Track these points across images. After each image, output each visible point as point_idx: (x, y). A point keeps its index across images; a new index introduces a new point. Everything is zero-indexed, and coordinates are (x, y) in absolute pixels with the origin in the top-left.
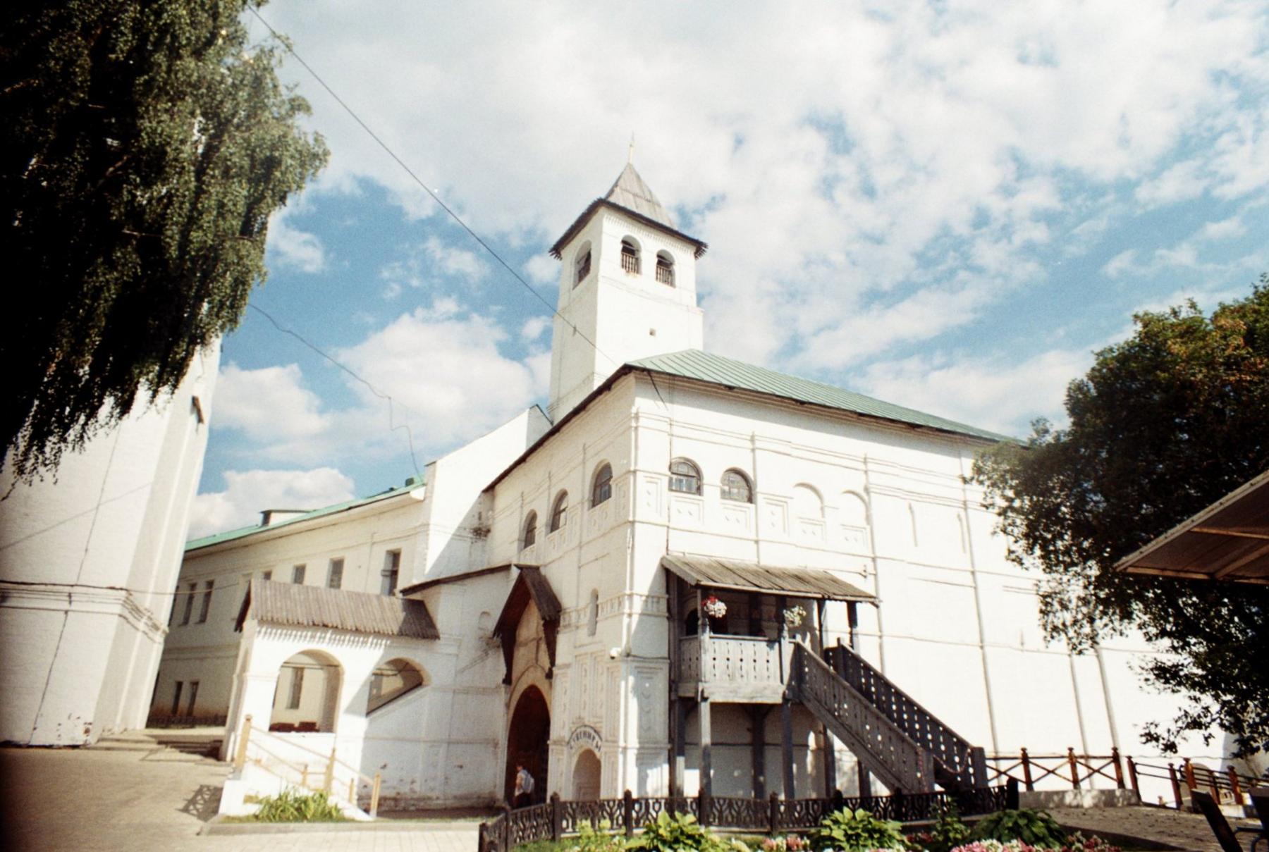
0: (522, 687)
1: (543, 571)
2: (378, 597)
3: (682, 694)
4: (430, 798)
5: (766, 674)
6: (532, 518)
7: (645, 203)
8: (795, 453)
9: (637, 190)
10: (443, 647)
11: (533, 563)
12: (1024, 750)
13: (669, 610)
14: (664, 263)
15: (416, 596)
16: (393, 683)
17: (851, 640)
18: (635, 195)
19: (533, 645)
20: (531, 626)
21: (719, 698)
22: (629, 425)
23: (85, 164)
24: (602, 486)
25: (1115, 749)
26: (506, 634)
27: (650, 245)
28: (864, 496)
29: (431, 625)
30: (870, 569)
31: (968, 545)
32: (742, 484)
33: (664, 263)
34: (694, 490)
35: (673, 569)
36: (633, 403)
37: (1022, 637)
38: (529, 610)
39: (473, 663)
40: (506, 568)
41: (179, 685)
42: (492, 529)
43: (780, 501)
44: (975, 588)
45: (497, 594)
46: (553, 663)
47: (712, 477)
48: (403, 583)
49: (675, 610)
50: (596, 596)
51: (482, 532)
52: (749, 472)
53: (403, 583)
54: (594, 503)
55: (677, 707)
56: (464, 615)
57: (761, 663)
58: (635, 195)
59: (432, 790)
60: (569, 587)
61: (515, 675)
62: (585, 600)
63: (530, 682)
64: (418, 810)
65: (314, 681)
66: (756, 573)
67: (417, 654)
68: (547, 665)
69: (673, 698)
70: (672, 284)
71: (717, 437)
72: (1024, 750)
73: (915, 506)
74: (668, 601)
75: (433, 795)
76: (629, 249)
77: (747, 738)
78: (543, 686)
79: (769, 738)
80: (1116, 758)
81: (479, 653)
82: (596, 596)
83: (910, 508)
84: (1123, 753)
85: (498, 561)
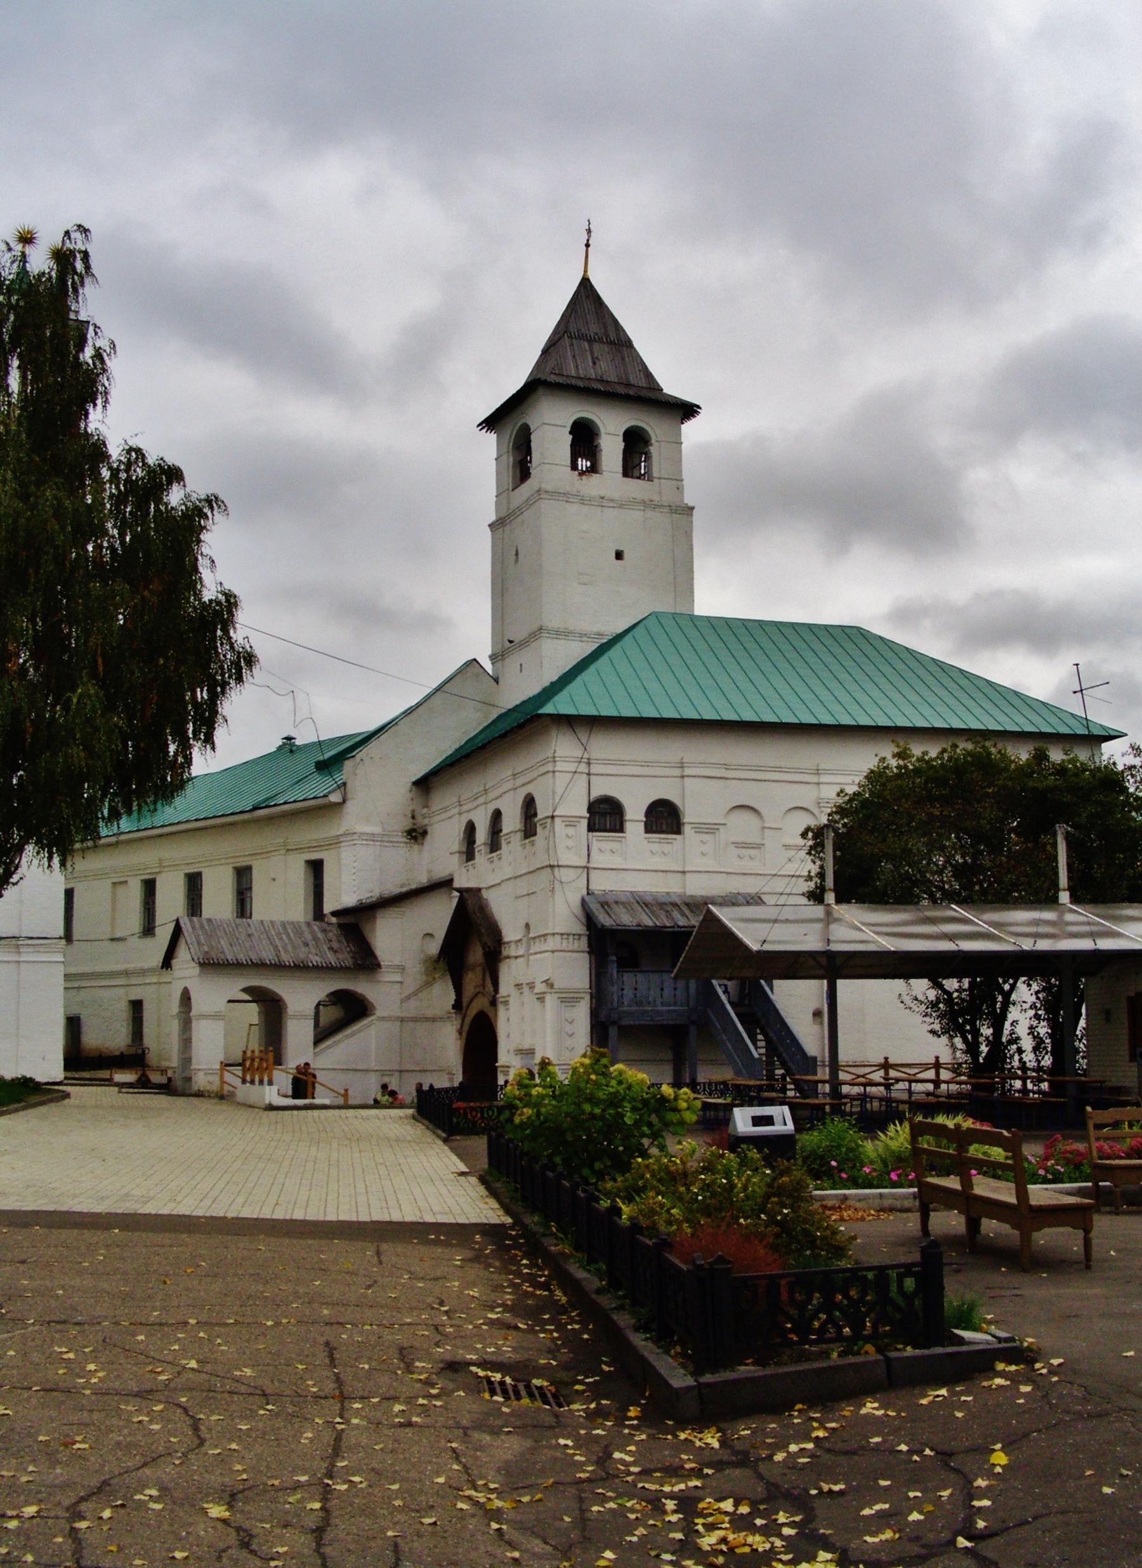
0: (472, 1012)
1: (485, 894)
2: (308, 924)
10: (387, 976)
11: (472, 884)
12: (937, 1058)
13: (590, 945)
14: (636, 444)
15: (349, 920)
19: (479, 970)
20: (476, 955)
23: (74, 691)
38: (471, 945)
43: (709, 829)
45: (437, 916)
46: (496, 990)
53: (328, 908)
56: (405, 941)
61: (465, 1000)
64: (27, 1225)
67: (361, 987)
71: (635, 774)
72: (937, 1058)
76: (584, 439)
77: (669, 1055)
85: (441, 873)
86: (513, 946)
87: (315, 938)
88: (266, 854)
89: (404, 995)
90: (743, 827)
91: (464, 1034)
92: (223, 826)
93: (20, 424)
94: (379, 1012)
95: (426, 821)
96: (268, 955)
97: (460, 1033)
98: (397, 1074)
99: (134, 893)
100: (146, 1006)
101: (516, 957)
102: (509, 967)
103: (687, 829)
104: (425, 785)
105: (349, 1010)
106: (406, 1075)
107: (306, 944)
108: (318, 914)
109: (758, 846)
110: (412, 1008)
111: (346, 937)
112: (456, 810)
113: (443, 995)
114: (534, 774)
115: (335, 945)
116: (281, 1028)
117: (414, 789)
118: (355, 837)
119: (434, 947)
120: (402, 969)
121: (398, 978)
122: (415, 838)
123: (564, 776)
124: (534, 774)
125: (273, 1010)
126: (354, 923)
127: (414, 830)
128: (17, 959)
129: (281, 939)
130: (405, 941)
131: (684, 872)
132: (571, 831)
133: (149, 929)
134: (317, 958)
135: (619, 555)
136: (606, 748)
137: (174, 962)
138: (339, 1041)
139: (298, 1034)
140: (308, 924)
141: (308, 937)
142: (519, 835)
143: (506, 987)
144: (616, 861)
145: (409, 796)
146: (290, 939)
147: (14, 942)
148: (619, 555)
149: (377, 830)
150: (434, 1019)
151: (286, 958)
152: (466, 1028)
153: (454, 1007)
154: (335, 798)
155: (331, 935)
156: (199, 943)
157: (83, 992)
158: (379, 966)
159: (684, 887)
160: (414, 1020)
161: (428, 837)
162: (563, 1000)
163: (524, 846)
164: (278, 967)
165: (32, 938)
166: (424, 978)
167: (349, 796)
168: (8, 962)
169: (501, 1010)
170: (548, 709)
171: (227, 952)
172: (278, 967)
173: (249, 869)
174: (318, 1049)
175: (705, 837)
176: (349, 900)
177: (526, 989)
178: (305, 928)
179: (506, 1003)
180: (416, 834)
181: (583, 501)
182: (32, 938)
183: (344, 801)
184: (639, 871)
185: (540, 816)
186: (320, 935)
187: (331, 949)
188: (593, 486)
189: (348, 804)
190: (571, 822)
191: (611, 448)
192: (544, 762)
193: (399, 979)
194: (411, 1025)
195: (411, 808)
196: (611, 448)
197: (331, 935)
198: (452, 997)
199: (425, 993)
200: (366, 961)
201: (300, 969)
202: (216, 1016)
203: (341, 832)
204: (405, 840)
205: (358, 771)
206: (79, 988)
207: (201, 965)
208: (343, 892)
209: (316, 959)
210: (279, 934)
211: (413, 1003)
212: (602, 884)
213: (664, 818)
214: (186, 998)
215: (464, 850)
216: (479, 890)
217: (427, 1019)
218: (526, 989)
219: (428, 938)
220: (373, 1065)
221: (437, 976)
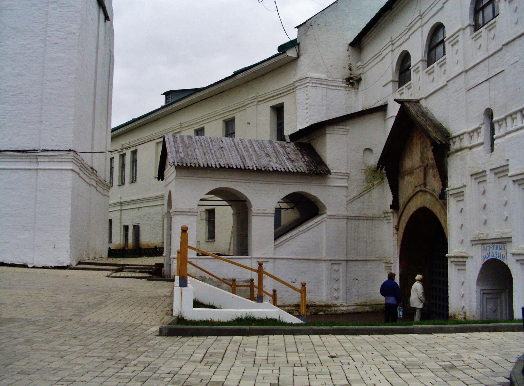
0: (412, 207)
1: (423, 103)
2: (271, 142)
4: (335, 306)
10: (334, 181)
19: (419, 174)
20: (415, 158)
26: (390, 165)
40: (383, 109)
41: (126, 228)
42: (363, 77)
45: (377, 135)
48: (288, 131)
50: (489, 114)
51: (353, 81)
53: (288, 131)
54: (476, 27)
56: (349, 153)
59: (337, 298)
61: (402, 200)
62: (477, 120)
65: (225, 215)
67: (313, 190)
75: (338, 302)
78: (436, 209)
82: (489, 114)
86: (466, 137)
87: (276, 152)
88: (243, 107)
89: (349, 199)
91: (401, 231)
94: (329, 212)
95: (360, 71)
96: (235, 161)
97: (397, 230)
98: (344, 263)
101: (470, 148)
102: (462, 159)
104: (358, 44)
105: (305, 209)
106: (350, 263)
107: (268, 155)
108: (280, 136)
110: (356, 209)
111: (300, 151)
112: (389, 49)
115: (293, 157)
117: (350, 48)
118: (308, 80)
119: (373, 160)
120: (347, 176)
121: (344, 183)
122: (352, 84)
125: (241, 206)
126: (308, 140)
127: (351, 78)
128: (36, 167)
129: (248, 151)
130: (349, 153)
134: (277, 165)
138: (297, 235)
139: (261, 228)
140: (271, 142)
141: (270, 150)
142: (468, 30)
143: (454, 181)
145: (347, 53)
146: (255, 151)
147: (34, 154)
149: (323, 76)
150: (373, 218)
151: (250, 164)
152: (403, 225)
153: (392, 207)
155: (288, 150)
156: (177, 152)
157: (141, 210)
158: (329, 172)
160: (358, 218)
161: (362, 83)
163: (475, 39)
164: (243, 171)
165: (47, 151)
166: (365, 184)
167: (302, 52)
168: (29, 169)
169: (452, 204)
171: (199, 158)
172: (243, 171)
173: (233, 120)
174: (278, 242)
176: (302, 124)
177: (490, 177)
178: (267, 144)
179: (459, 194)
180: (353, 81)
182: (47, 151)
186: (280, 149)
187: (288, 159)
189: (302, 58)
193: (346, 185)
194: (354, 222)
195: (348, 62)
197: (288, 150)
198: (389, 198)
199: (366, 196)
200: (319, 170)
201: (262, 173)
203: (297, 79)
204: (344, 85)
205: (308, 33)
206: (139, 208)
208: (296, 122)
209: (275, 165)
210: (246, 147)
211: (357, 205)
215: (397, 79)
216: (418, 101)
217: (368, 218)
218: (490, 177)
219: (368, 153)
220: (324, 256)
221: (375, 183)
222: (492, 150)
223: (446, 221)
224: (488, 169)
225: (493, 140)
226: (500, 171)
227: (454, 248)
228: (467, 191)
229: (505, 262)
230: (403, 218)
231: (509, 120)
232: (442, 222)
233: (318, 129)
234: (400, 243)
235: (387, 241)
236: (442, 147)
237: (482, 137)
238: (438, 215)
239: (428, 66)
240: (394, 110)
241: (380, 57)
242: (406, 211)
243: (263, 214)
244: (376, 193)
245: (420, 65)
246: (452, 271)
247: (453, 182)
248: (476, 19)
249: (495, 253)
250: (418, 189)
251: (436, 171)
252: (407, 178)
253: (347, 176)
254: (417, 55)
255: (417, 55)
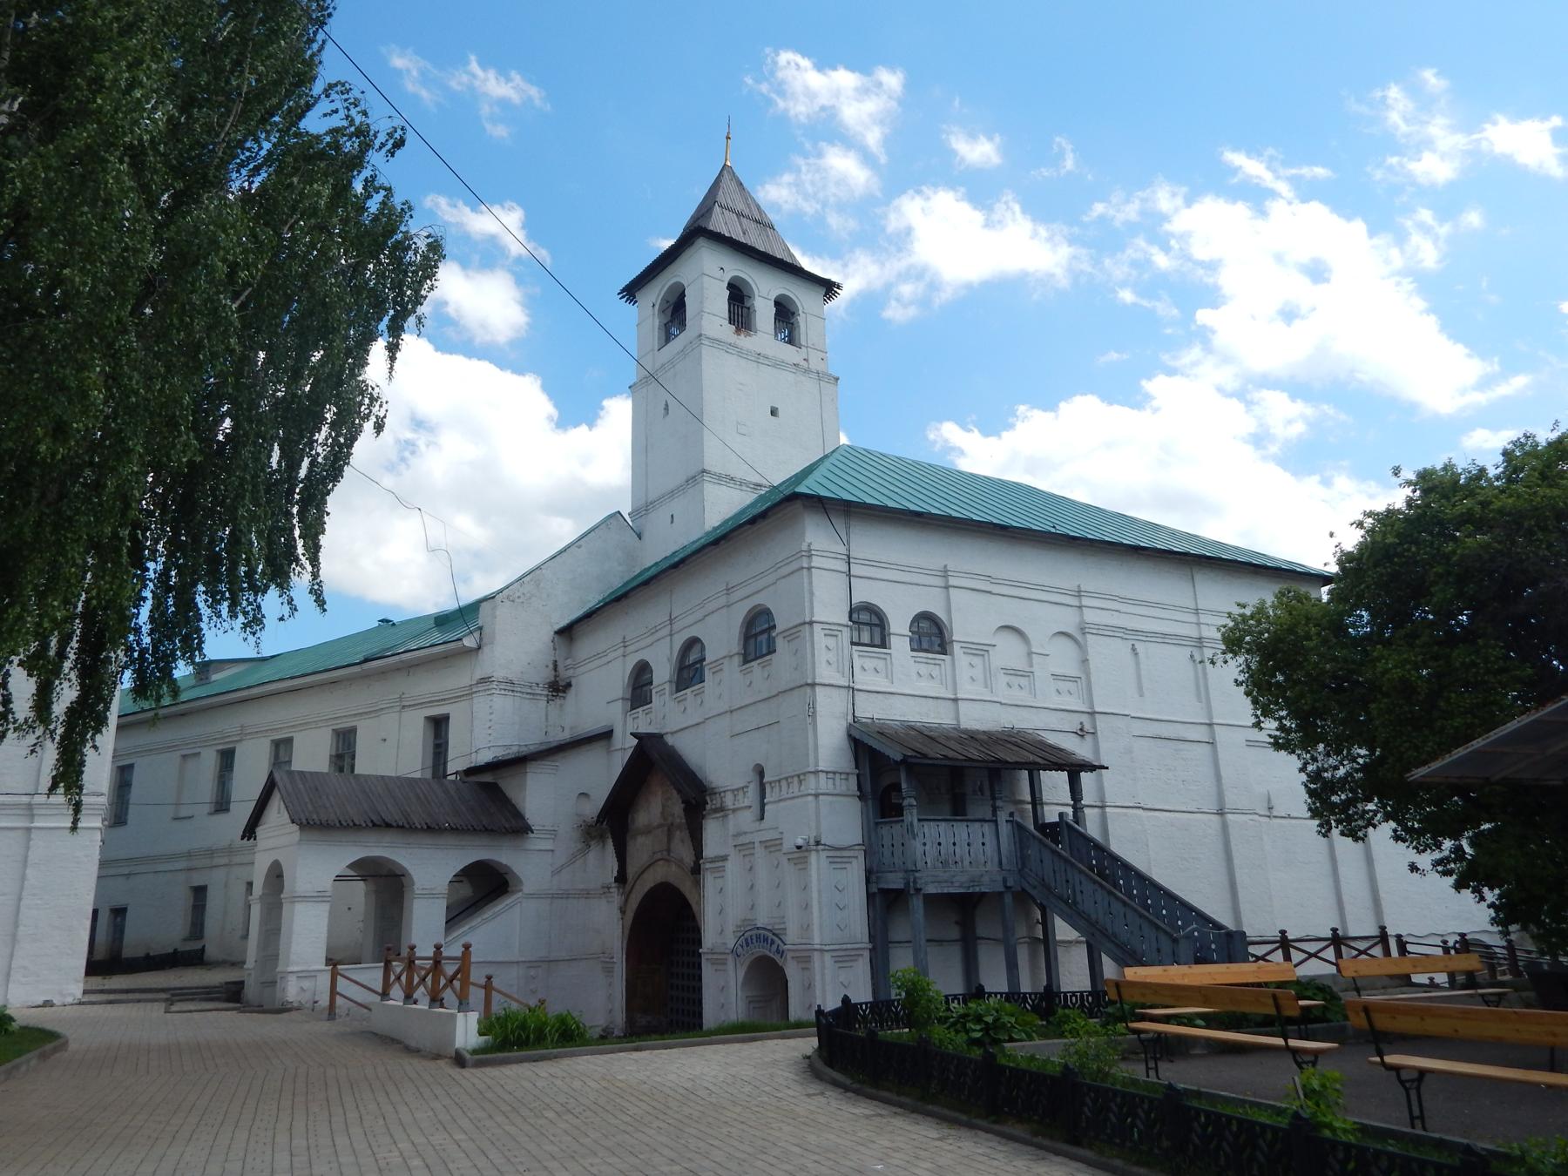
3: (883, 886)
5: (982, 860)
6: (643, 669)
7: (753, 225)
8: (995, 589)
9: (740, 207)
10: (536, 843)
12: (1283, 932)
14: (785, 313)
15: (487, 778)
16: (894, 881)
17: (1075, 813)
18: (739, 215)
20: (656, 808)
21: (932, 889)
22: (801, 564)
24: (759, 636)
25: (1383, 928)
26: (614, 820)
27: (766, 289)
28: (1076, 637)
29: (518, 815)
30: (1087, 727)
31: (1202, 692)
32: (932, 634)
33: (785, 313)
34: (877, 641)
35: (867, 740)
36: (803, 534)
37: (1269, 801)
39: (572, 860)
40: (606, 735)
43: (980, 650)
44: (1212, 744)
45: (599, 775)
47: (899, 624)
49: (868, 787)
51: (558, 688)
52: (941, 614)
54: (746, 659)
55: (878, 900)
56: (555, 800)
57: (977, 845)
58: (739, 215)
60: (717, 757)
61: (631, 871)
63: (659, 879)
66: (960, 741)
67: (503, 855)
68: (688, 858)
69: (874, 889)
70: (791, 340)
71: (899, 575)
72: (1283, 932)
73: (1138, 646)
74: (858, 776)
76: (738, 296)
77: (954, 932)
78: (686, 887)
79: (981, 930)
80: (1383, 937)
81: (580, 846)
82: (760, 772)
83: (1134, 649)
84: (1391, 931)
85: (590, 725)
90: (1008, 652)
91: (630, 915)
92: (322, 685)
93: (154, 551)
94: (529, 886)
95: (570, 672)
99: (209, 761)
100: (211, 893)
101: (734, 810)
103: (956, 647)
104: (567, 633)
105: (484, 887)
109: (1028, 674)
112: (621, 651)
113: (602, 863)
114: (771, 578)
116: (401, 909)
119: (593, 808)
120: (553, 834)
121: (548, 845)
122: (557, 690)
123: (827, 576)
124: (771, 578)
125: (388, 886)
130: (555, 800)
131: (956, 700)
132: (831, 642)
133: (222, 805)
135: (774, 412)
136: (870, 544)
137: (260, 831)
142: (737, 660)
144: (881, 684)
148: (774, 412)
153: (617, 880)
154: (469, 642)
159: (958, 719)
162: (832, 861)
169: (710, 882)
170: (802, 489)
175: (977, 661)
177: (759, 851)
180: (558, 688)
181: (742, 353)
183: (479, 648)
184: (908, 694)
185: (779, 629)
188: (744, 341)
189: (486, 649)
190: (831, 630)
191: (764, 312)
192: (798, 555)
196: (764, 312)
200: (516, 827)
202: (319, 897)
207: (301, 826)
212: (870, 710)
213: (932, 634)
214: (276, 875)
215: (628, 696)
218: (759, 851)
222: (762, 818)
223: (699, 903)
224: (757, 840)
225: (763, 806)
226: (772, 845)
227: (709, 938)
228: (729, 865)
229: (780, 962)
230: (633, 896)
231: (784, 783)
232: (694, 906)
233: (517, 763)
234: (627, 932)
235: (606, 924)
236: (697, 799)
237: (751, 797)
238: (688, 896)
239: (678, 690)
240: (625, 744)
241: (605, 660)
242: (637, 887)
243: (432, 895)
244: (593, 856)
245: (667, 686)
246: (707, 972)
247: (710, 850)
248: (745, 646)
249: (760, 950)
250: (659, 856)
251: (686, 834)
252: (641, 840)
253: (553, 834)
254: (663, 673)
255: (663, 673)
